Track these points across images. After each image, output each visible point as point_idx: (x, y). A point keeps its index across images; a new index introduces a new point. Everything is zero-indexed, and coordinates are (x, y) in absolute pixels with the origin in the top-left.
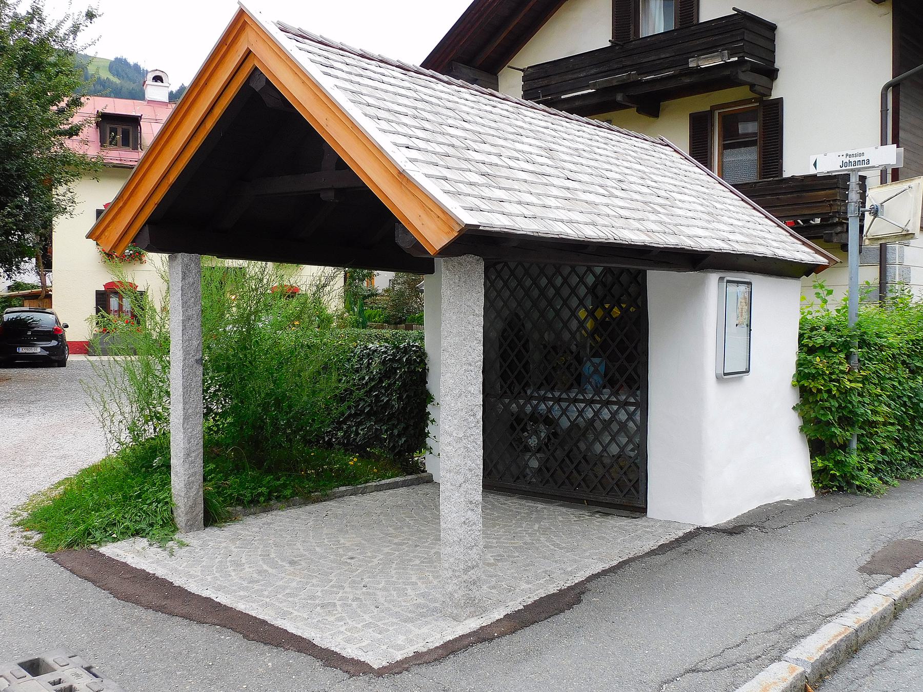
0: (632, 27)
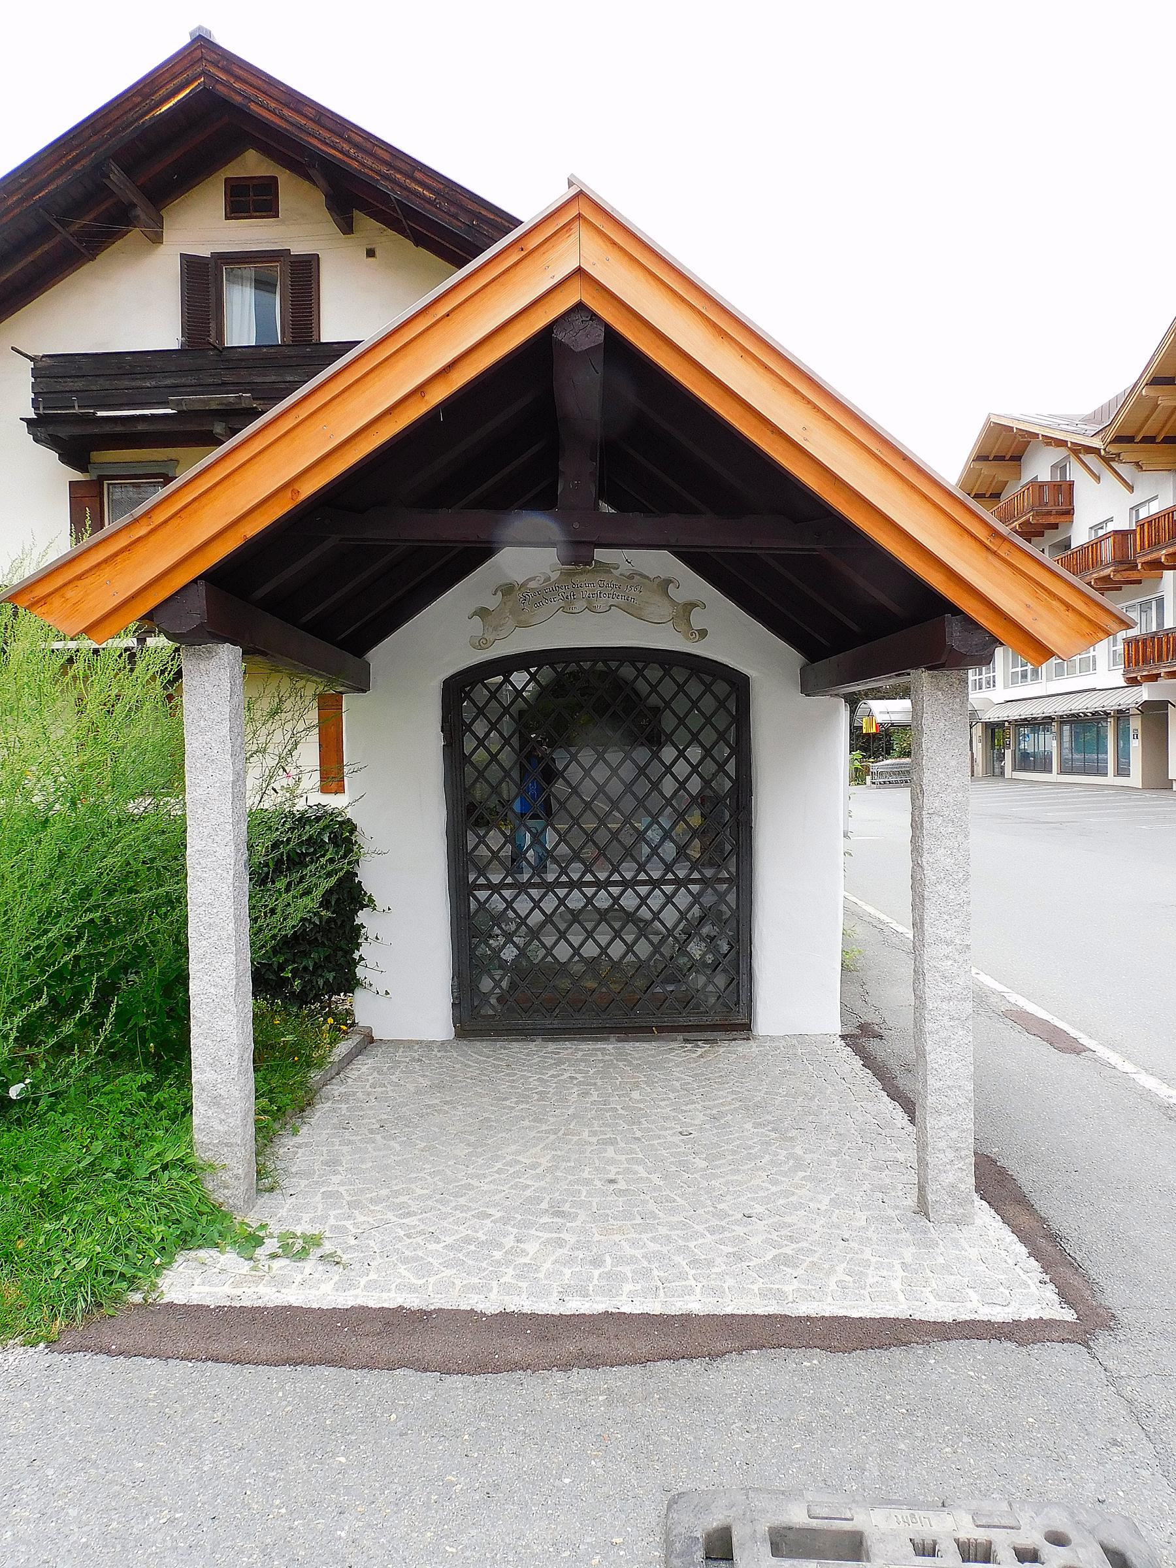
0: (212, 325)
